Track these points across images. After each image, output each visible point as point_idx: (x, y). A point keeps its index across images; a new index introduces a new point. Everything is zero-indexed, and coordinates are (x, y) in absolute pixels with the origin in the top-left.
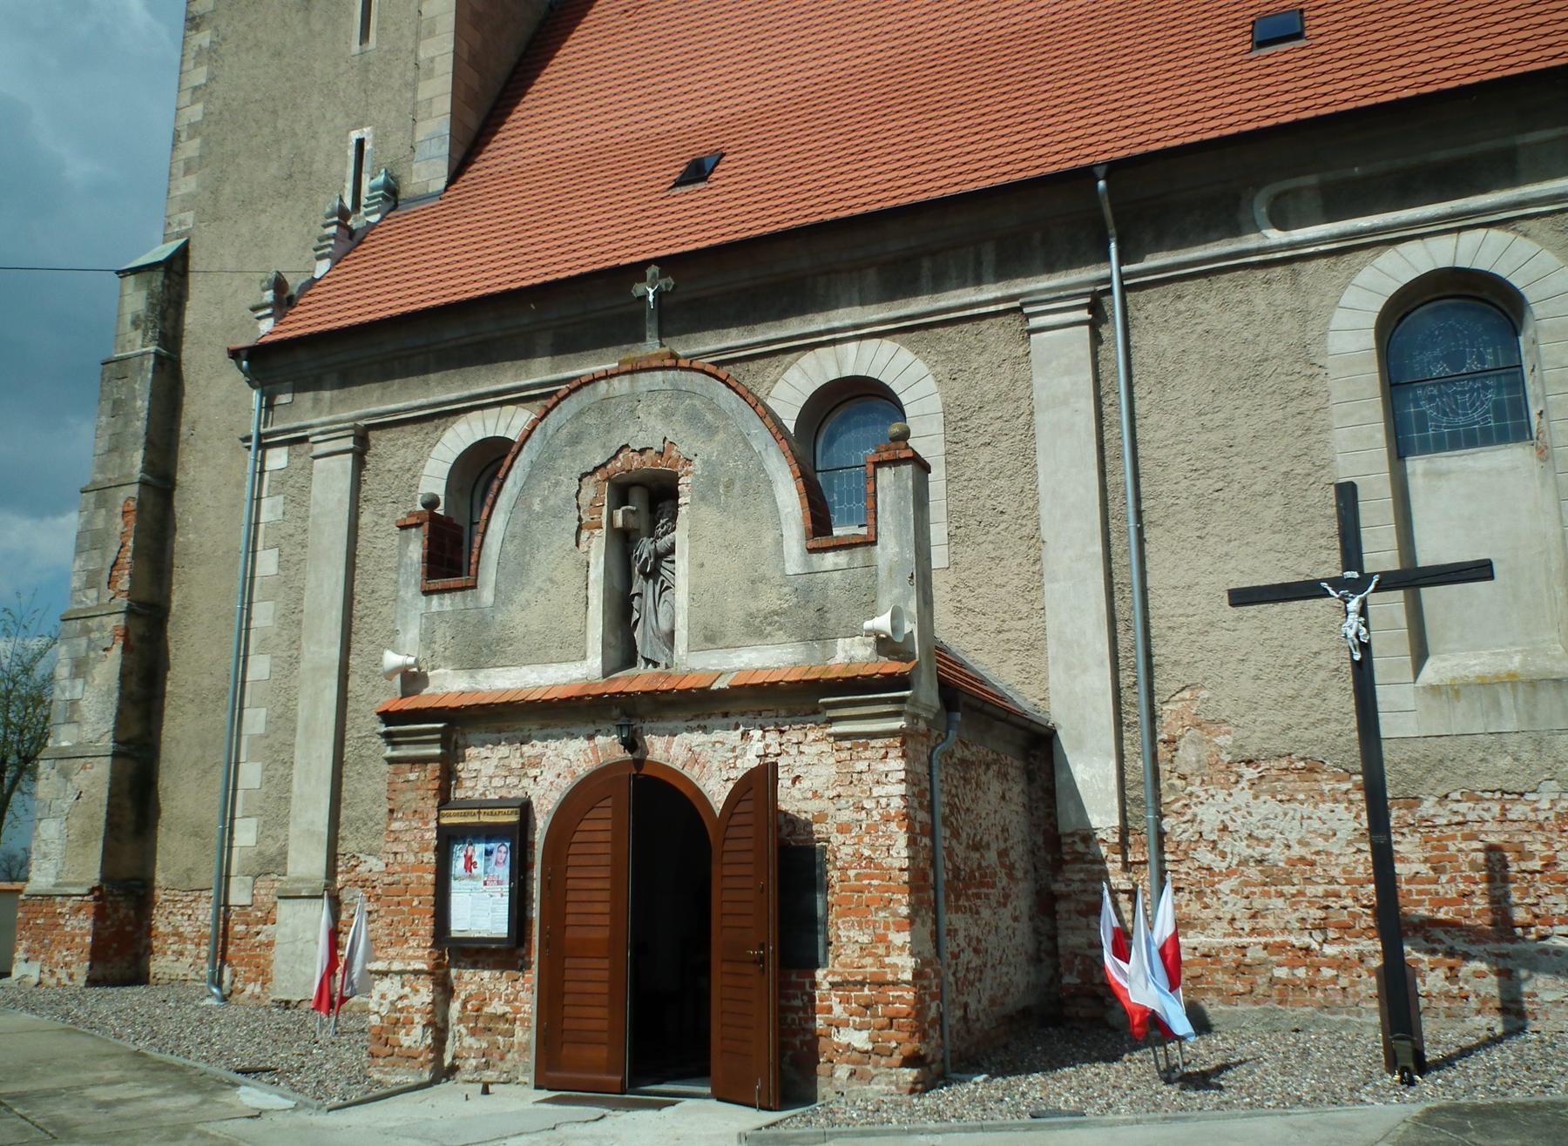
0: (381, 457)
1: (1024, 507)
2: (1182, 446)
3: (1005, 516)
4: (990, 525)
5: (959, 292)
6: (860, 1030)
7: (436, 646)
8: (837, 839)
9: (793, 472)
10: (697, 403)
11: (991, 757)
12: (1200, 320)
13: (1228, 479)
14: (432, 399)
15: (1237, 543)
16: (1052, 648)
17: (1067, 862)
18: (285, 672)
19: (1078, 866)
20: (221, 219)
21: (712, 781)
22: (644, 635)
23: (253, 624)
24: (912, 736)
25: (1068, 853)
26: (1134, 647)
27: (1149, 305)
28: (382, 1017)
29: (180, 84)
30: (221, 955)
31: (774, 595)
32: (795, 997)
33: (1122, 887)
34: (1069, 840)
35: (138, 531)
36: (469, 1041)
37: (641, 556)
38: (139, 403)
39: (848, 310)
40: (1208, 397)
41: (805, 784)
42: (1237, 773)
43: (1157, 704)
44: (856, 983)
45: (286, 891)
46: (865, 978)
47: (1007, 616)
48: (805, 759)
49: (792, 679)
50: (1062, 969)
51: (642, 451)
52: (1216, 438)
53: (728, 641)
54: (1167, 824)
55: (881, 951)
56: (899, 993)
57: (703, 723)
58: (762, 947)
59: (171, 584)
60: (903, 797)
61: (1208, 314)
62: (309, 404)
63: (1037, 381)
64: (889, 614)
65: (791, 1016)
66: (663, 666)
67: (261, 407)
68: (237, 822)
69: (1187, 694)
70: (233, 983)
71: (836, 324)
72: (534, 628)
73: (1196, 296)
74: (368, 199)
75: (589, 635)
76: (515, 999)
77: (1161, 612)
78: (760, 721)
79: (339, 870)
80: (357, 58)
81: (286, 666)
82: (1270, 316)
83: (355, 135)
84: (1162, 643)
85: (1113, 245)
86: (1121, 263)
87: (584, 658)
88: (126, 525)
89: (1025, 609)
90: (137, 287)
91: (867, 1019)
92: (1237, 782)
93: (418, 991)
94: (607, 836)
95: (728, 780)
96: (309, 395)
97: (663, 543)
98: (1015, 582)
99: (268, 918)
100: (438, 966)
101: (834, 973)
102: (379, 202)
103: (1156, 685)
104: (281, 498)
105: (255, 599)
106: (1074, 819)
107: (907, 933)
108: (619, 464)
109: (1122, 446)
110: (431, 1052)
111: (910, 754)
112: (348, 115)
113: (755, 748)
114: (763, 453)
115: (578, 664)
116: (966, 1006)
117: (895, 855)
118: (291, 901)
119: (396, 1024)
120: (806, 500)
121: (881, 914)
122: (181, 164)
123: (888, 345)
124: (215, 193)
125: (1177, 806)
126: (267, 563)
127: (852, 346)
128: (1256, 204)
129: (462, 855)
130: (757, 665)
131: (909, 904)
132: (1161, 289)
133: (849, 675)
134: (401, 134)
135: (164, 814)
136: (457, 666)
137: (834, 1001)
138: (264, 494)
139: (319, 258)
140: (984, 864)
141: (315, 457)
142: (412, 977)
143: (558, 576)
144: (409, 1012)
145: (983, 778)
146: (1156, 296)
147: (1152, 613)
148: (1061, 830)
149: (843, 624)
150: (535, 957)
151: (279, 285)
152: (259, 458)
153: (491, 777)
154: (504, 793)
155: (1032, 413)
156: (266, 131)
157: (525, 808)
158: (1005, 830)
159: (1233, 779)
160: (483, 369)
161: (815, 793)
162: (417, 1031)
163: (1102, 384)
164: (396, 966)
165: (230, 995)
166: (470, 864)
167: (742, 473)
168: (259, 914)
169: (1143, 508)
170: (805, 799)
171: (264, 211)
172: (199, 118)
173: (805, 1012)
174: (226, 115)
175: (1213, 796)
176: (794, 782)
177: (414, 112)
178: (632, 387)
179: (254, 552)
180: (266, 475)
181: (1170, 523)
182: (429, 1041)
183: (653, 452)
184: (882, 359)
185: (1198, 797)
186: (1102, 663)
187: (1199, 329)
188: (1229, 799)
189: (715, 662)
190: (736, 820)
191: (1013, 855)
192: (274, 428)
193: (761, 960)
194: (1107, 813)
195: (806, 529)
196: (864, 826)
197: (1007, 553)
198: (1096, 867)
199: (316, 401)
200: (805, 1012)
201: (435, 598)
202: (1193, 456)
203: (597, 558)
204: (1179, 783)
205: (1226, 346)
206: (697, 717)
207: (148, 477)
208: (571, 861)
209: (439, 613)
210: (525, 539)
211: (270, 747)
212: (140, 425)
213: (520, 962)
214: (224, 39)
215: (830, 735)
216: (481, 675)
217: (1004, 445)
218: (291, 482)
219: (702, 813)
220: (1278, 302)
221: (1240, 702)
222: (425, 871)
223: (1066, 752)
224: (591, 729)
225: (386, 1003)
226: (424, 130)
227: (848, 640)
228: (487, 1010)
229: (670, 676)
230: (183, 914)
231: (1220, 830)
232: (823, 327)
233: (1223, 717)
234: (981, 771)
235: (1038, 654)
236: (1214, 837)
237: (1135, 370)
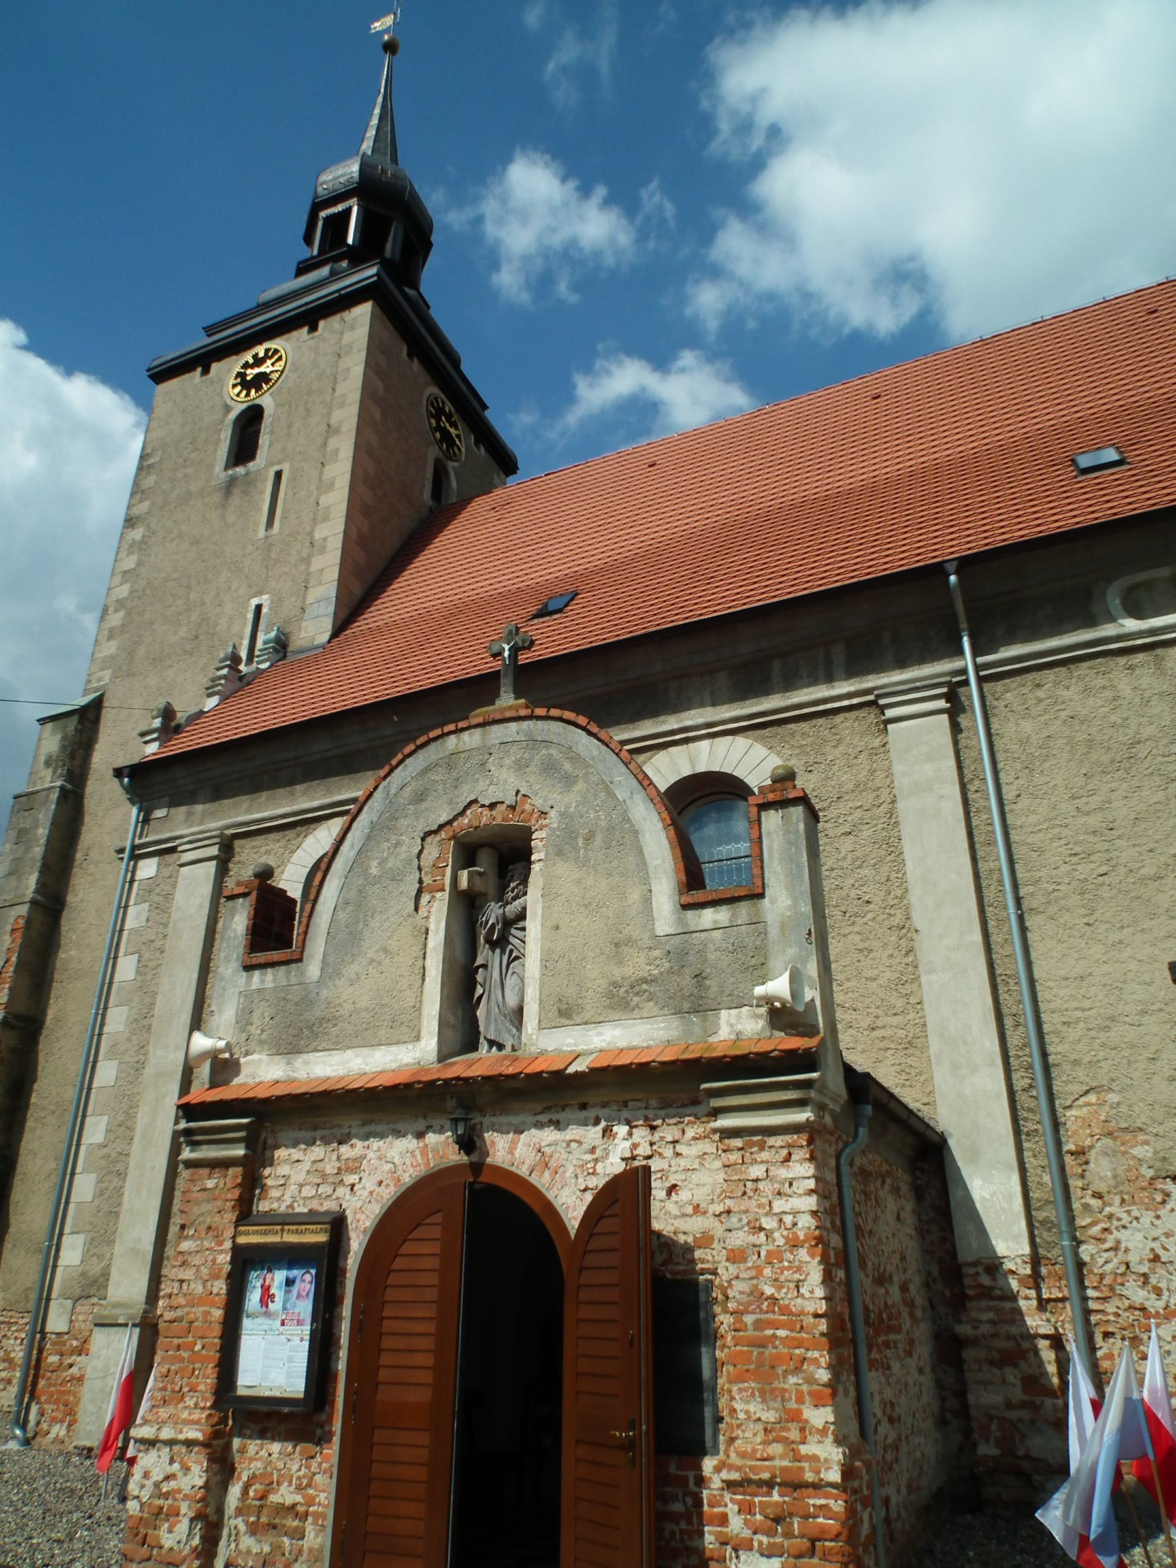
0: (244, 863)
1: (892, 896)
2: (1057, 830)
3: (872, 906)
4: (856, 915)
5: (811, 689)
6: (769, 1556)
7: (252, 1029)
8: (726, 1271)
9: (663, 820)
10: (553, 751)
11: (885, 1167)
12: (1063, 707)
13: (1112, 863)
14: (296, 808)
15: (1130, 930)
16: (934, 1045)
17: (970, 1298)
18: (130, 1079)
19: (984, 1303)
20: (133, 675)
21: (566, 1191)
22: (488, 1012)
23: (106, 1029)
24: (819, 1132)
25: (970, 1287)
26: (1026, 1045)
27: (1009, 694)
28: (142, 1505)
29: (113, 569)
30: (30, 1390)
31: (642, 960)
32: (675, 1498)
33: (1042, 1331)
34: (971, 1271)
35: (22, 947)
36: (247, 1542)
37: (487, 922)
38: (41, 831)
39: (699, 711)
40: (1080, 780)
41: (684, 1195)
42: (1163, 1191)
43: (1059, 1110)
44: (761, 1483)
45: (103, 1317)
46: (774, 1477)
47: (880, 1012)
48: (683, 1162)
49: (667, 1059)
50: (976, 1436)
51: (492, 806)
52: (1094, 821)
53: (587, 1015)
54: (1085, 1252)
55: (794, 1435)
56: (822, 1502)
57: (555, 1117)
58: (632, 1425)
59: (48, 998)
60: (814, 1213)
61: (1071, 701)
62: (182, 817)
63: (897, 769)
64: (787, 975)
65: (669, 1527)
66: (509, 1048)
67: (137, 822)
68: (65, 1238)
69: (1092, 1098)
70: (38, 1423)
71: (689, 723)
72: (363, 1004)
73: (1056, 684)
74: (260, 650)
75: (425, 1012)
76: (309, 1485)
77: (1052, 1006)
78: (625, 1114)
79: (162, 1294)
80: (262, 541)
81: (132, 1071)
82: (1137, 700)
83: (255, 602)
84: (1056, 1040)
85: (966, 640)
86: (975, 654)
87: (418, 1038)
88: (13, 942)
89: (900, 1004)
90: (53, 733)
91: (779, 1540)
92: (1164, 1202)
93: (188, 1469)
94: (434, 1263)
95: (585, 1190)
96: (183, 809)
97: (512, 909)
98: (888, 974)
99: (81, 1350)
100: (216, 1434)
101: (731, 1467)
102: (270, 652)
103: (1055, 1088)
104: (146, 905)
105: (110, 1005)
106: (975, 1245)
107: (829, 1409)
108: (466, 821)
109: (994, 832)
110: (197, 1558)
111: (818, 1154)
112: (250, 586)
113: (620, 1148)
114: (628, 802)
115: (410, 1047)
116: (886, 1501)
117: (807, 1295)
118: (107, 1329)
119: (158, 1514)
120: (678, 850)
121: (792, 1380)
122: (106, 632)
123: (741, 742)
124: (131, 654)
125: (1095, 1230)
126: (126, 968)
127: (705, 744)
128: (1109, 598)
129: (259, 1284)
130: (622, 1044)
131: (830, 1367)
132: (1018, 679)
133: (738, 1053)
134: (294, 599)
135: (12, 1230)
136: (274, 1051)
137: (731, 1509)
138: (131, 903)
139: (209, 695)
140: (890, 1302)
141: (182, 865)
142: (184, 1450)
143: (393, 945)
144: (175, 1499)
145: (881, 1193)
146: (1014, 686)
147: (1042, 1007)
148: (960, 1258)
149: (727, 992)
150: (337, 1426)
151: (168, 713)
152: (131, 868)
153: (301, 1186)
154: (314, 1205)
155: (893, 802)
156: (180, 602)
157: (338, 1224)
158: (903, 1258)
159: (1159, 1198)
160: (346, 779)
161: (697, 1208)
162: (183, 1526)
163: (966, 771)
164: (166, 1434)
165: (34, 1438)
166: (267, 1296)
167: (604, 824)
168: (75, 1343)
169: (1021, 894)
170: (684, 1215)
171: (171, 666)
172: (126, 595)
173: (689, 1522)
174: (148, 591)
175: (1137, 1218)
176: (669, 1193)
177: (307, 581)
178: (483, 739)
179: (116, 958)
180: (136, 884)
181: (1052, 909)
182: (196, 1541)
183: (504, 806)
184: (735, 755)
185: (1119, 1219)
186: (993, 1063)
187: (1063, 714)
188: (1156, 1222)
189: (570, 1041)
190: (595, 1244)
191: (912, 1288)
192: (148, 839)
193: (630, 1445)
194: (1015, 1238)
195: (679, 883)
196: (763, 1254)
197: (876, 944)
198: (1007, 1305)
199: (189, 814)
200: (689, 1522)
201: (257, 974)
202: (1070, 839)
203: (438, 923)
204: (1095, 1202)
205: (1093, 731)
206: (548, 1109)
207: (39, 898)
208: (390, 1295)
209: (259, 990)
210: (359, 905)
211: (108, 1156)
212: (38, 851)
213: (319, 1432)
214: (154, 533)
215: (715, 1131)
216: (299, 1061)
217: (865, 834)
218: (158, 890)
219: (552, 1233)
220: (1144, 687)
221: (1157, 1107)
222: (213, 1304)
223: (960, 1164)
224: (421, 1125)
225: (149, 1484)
226: (313, 595)
227: (733, 1012)
228: (274, 1498)
229: (516, 1059)
230: (16, 1338)
231: (1150, 1261)
232: (676, 726)
233: (1139, 1124)
234: (878, 1184)
235: (918, 1053)
236: (1144, 1269)
237: (1000, 757)
